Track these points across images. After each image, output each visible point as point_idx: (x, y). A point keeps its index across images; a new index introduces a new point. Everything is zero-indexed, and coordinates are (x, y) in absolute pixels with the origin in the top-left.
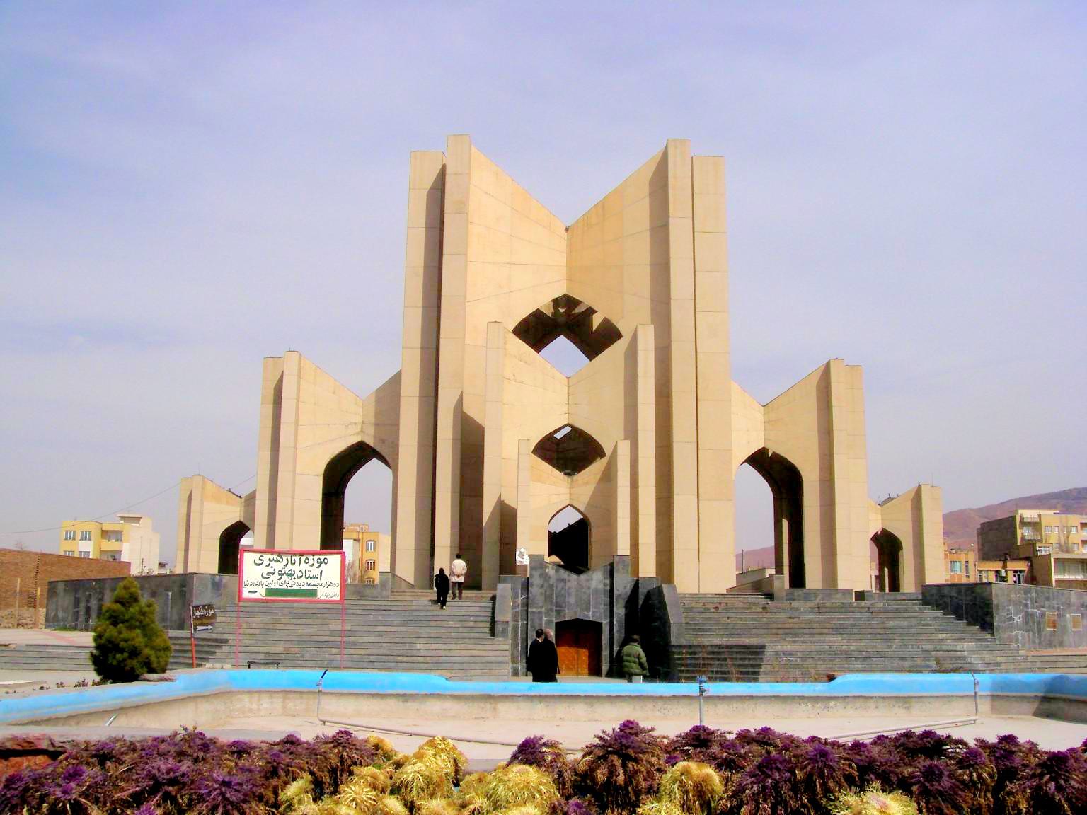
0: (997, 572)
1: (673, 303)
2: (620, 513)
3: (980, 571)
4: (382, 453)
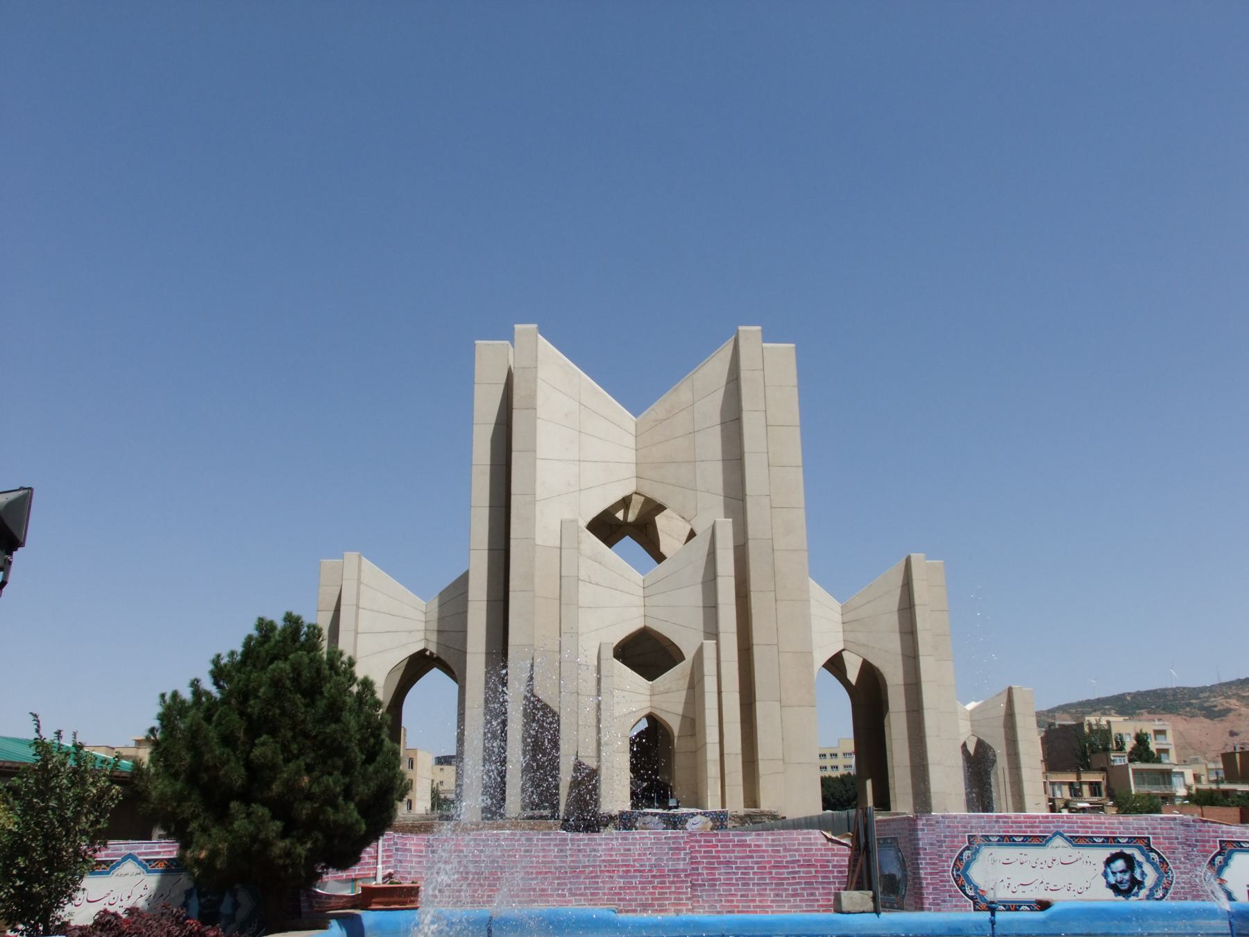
0: (1071, 784)
1: (748, 499)
2: (483, 606)
3: (1053, 784)
4: (449, 663)
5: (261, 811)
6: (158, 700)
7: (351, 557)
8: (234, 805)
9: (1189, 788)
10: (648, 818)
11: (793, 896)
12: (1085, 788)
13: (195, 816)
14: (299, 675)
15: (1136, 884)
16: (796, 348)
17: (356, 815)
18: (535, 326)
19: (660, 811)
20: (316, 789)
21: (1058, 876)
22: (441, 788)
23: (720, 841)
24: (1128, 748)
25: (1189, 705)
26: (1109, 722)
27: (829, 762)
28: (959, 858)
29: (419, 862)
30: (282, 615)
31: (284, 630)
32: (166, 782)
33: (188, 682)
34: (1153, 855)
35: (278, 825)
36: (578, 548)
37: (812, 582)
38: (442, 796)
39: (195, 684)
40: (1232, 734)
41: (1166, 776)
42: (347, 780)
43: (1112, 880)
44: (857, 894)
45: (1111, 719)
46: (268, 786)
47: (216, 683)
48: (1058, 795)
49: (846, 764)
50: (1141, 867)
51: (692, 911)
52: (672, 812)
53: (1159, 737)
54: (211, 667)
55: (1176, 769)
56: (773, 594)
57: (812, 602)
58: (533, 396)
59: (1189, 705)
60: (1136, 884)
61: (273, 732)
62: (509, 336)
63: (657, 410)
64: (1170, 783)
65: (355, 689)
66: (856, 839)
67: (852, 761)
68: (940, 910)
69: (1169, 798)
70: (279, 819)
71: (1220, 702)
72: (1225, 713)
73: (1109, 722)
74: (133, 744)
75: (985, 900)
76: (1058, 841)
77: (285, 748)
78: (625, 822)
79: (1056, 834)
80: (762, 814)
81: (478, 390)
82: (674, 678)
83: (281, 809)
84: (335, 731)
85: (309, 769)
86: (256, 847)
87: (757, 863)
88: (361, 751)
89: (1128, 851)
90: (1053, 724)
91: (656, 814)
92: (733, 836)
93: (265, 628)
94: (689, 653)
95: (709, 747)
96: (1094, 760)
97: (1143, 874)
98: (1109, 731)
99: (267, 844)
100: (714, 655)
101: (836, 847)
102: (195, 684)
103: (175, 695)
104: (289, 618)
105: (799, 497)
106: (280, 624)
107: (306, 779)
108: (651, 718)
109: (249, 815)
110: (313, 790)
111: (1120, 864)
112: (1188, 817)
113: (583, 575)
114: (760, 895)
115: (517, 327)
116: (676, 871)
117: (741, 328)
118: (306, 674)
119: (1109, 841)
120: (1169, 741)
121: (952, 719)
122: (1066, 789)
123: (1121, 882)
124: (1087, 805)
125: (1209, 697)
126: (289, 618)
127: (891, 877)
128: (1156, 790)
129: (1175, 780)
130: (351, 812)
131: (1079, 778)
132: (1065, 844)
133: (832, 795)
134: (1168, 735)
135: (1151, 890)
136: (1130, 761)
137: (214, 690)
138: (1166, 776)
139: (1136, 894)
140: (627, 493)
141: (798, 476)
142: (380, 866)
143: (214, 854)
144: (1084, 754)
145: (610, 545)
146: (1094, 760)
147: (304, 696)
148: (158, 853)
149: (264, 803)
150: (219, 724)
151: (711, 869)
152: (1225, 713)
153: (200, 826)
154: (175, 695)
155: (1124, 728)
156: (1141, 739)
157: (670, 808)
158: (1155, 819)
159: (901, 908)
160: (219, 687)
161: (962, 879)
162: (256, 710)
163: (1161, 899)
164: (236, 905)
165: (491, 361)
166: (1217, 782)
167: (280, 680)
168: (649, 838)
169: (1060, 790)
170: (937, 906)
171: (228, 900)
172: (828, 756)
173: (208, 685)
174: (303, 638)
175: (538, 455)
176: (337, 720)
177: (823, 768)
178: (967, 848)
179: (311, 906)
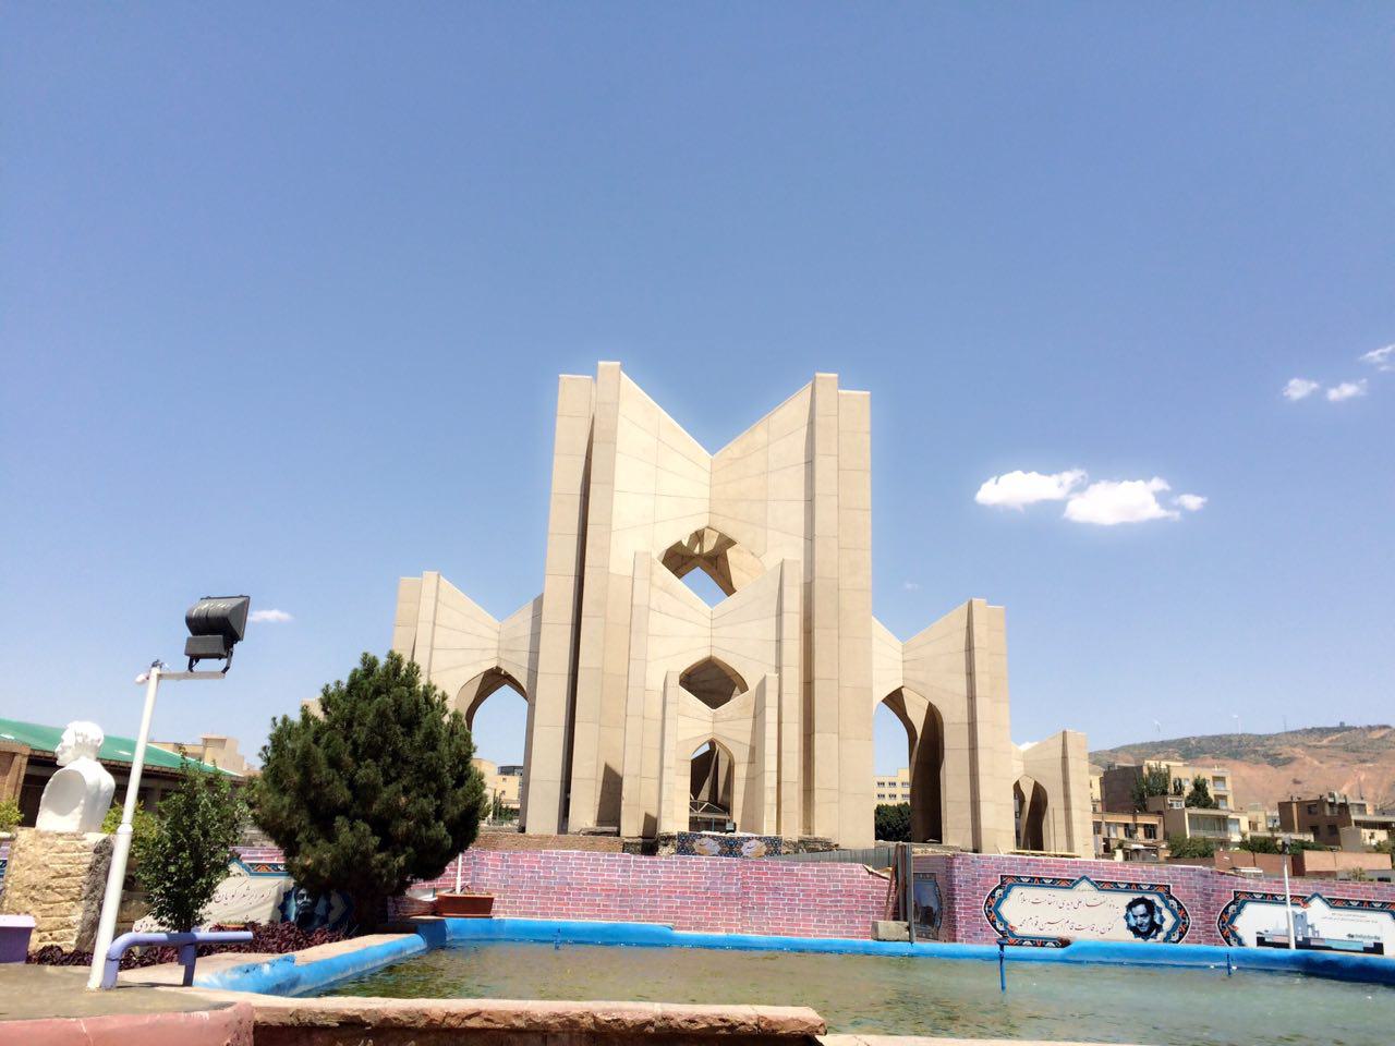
0: (1126, 825)
5: (363, 826)
6: (271, 722)
7: (430, 577)
8: (339, 820)
9: (1244, 835)
10: (705, 840)
11: (835, 922)
12: (1141, 831)
13: (302, 829)
14: (400, 706)
15: (1155, 927)
16: (872, 397)
17: (444, 832)
18: (618, 363)
19: (717, 834)
20: (412, 809)
21: (1082, 917)
22: (503, 798)
23: (770, 869)
24: (1186, 793)
25: (1255, 752)
26: (1168, 766)
27: (887, 790)
28: (992, 896)
29: (495, 876)
30: (386, 652)
31: (387, 666)
32: (277, 797)
33: (300, 708)
34: (1172, 902)
35: (375, 841)
36: (650, 580)
37: (876, 623)
38: (504, 806)
39: (305, 709)
40: (1296, 782)
41: (1223, 822)
42: (439, 802)
43: (1133, 922)
44: (893, 924)
45: (1172, 764)
46: (370, 804)
47: (324, 710)
48: (1113, 835)
49: (900, 795)
50: (1160, 911)
51: (741, 931)
52: (729, 835)
53: (1217, 783)
54: (321, 695)
55: (1232, 816)
56: (836, 632)
57: (874, 640)
58: (614, 432)
59: (1255, 752)
60: (1155, 927)
61: (376, 758)
62: (593, 371)
63: (733, 449)
64: (1226, 829)
65: (446, 719)
66: (895, 872)
67: (907, 791)
68: (971, 942)
69: (1225, 843)
70: (378, 835)
71: (1286, 751)
72: (1289, 761)
73: (1168, 766)
74: (200, 742)
75: (1014, 936)
76: (1084, 885)
77: (385, 773)
78: (684, 845)
79: (1082, 878)
80: (816, 841)
81: (561, 424)
82: (737, 704)
83: (380, 825)
84: (431, 758)
85: (406, 791)
86: (358, 857)
87: (803, 891)
88: (452, 777)
89: (1149, 897)
90: (1113, 765)
91: (713, 837)
92: (780, 863)
93: (369, 664)
94: (752, 684)
95: (767, 775)
96: (1152, 803)
97: (1162, 919)
98: (1168, 774)
99: (366, 856)
100: (776, 688)
101: (876, 880)
102: (305, 709)
103: (285, 720)
104: (391, 655)
105: (866, 538)
106: (383, 661)
107: (403, 800)
108: (712, 743)
109: (352, 829)
110: (409, 809)
111: (1141, 909)
112: (1207, 869)
113: (653, 605)
114: (804, 920)
115: (601, 363)
116: (728, 894)
117: (819, 375)
118: (405, 706)
119: (1130, 887)
120: (1227, 788)
121: (998, 763)
122: (1121, 830)
123: (1141, 925)
124: (1142, 847)
125: (1274, 745)
126: (391, 655)
127: (928, 909)
128: (1210, 836)
129: (1231, 827)
130: (440, 830)
131: (1135, 819)
132: (1092, 888)
133: (888, 824)
134: (1233, 783)
135: (1168, 933)
136: (1187, 806)
137: (320, 715)
138: (1223, 822)
139: (1155, 937)
140: (699, 527)
141: (865, 519)
142: (459, 878)
143: (320, 863)
144: (1142, 795)
145: (680, 576)
146: (1152, 803)
147: (403, 725)
148: (261, 858)
149: (365, 819)
150: (327, 746)
151: (760, 893)
152: (1289, 761)
153: (307, 837)
154: (285, 720)
155: (1183, 773)
156: (1200, 786)
157: (727, 832)
158: (1177, 869)
159: (936, 939)
160: (326, 713)
161: (993, 914)
162: (363, 737)
163: (1178, 942)
164: (329, 908)
165: (573, 391)
166: (1271, 830)
167: (384, 711)
168: (706, 863)
169: (1116, 831)
170: (970, 937)
171: (322, 903)
172: (887, 785)
173: (317, 711)
174: (403, 673)
175: (616, 488)
176: (434, 748)
177: (881, 796)
178: (1000, 887)
179: (397, 911)
